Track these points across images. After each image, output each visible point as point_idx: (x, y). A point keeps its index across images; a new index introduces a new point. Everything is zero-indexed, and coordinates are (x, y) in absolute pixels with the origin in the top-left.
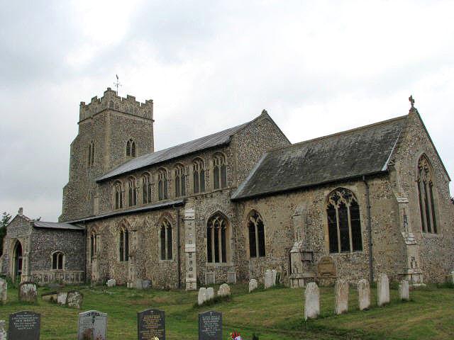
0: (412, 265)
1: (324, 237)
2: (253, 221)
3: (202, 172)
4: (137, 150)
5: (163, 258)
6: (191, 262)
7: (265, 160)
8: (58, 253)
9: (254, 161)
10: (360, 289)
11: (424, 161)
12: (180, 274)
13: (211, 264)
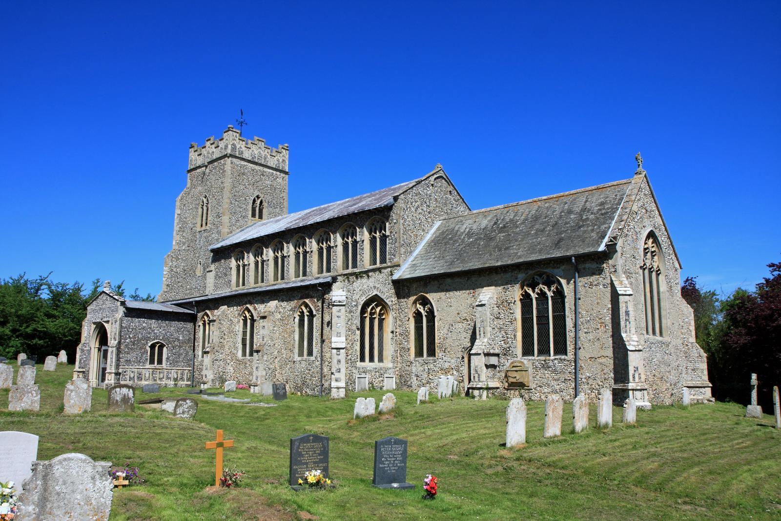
0: (634, 377)
1: (515, 336)
2: (422, 310)
3: (355, 243)
4: (264, 211)
5: (301, 354)
6: (339, 361)
7: (438, 229)
8: (157, 343)
9: (424, 230)
10: (576, 409)
11: (651, 240)
12: (322, 376)
13: (362, 364)
